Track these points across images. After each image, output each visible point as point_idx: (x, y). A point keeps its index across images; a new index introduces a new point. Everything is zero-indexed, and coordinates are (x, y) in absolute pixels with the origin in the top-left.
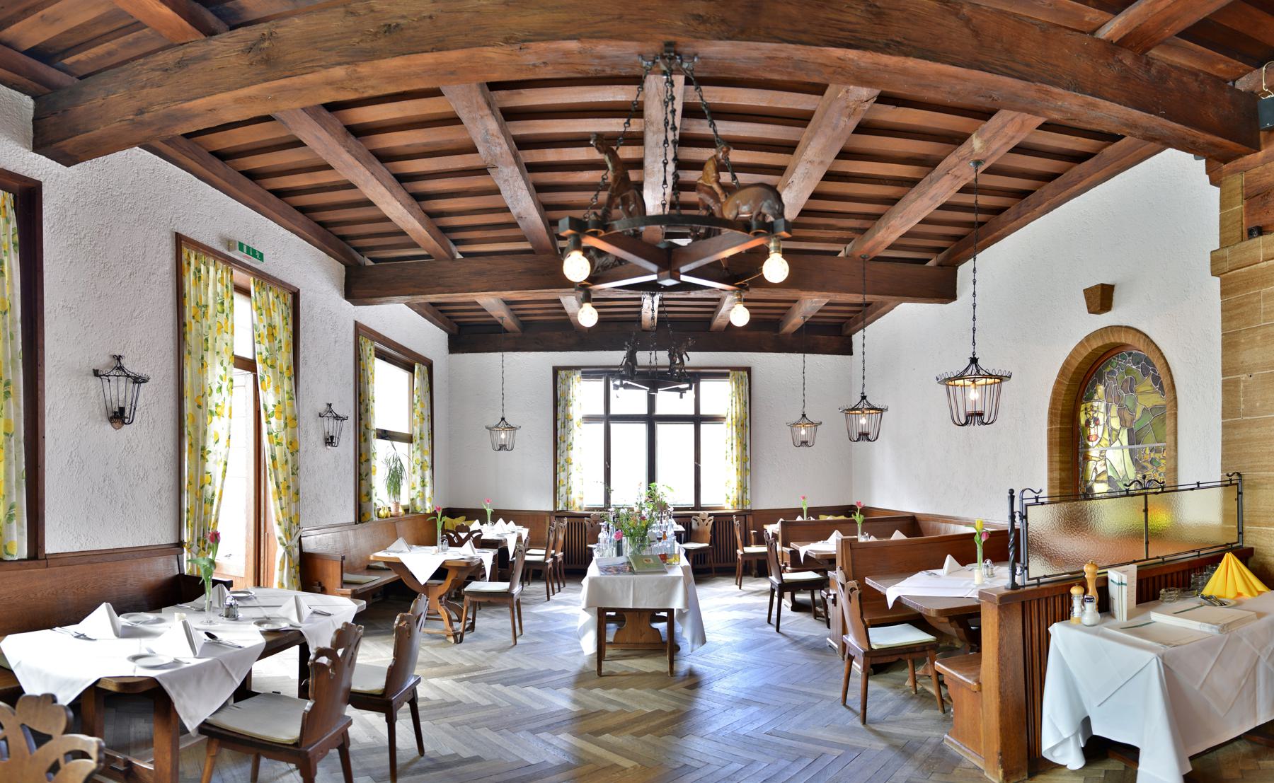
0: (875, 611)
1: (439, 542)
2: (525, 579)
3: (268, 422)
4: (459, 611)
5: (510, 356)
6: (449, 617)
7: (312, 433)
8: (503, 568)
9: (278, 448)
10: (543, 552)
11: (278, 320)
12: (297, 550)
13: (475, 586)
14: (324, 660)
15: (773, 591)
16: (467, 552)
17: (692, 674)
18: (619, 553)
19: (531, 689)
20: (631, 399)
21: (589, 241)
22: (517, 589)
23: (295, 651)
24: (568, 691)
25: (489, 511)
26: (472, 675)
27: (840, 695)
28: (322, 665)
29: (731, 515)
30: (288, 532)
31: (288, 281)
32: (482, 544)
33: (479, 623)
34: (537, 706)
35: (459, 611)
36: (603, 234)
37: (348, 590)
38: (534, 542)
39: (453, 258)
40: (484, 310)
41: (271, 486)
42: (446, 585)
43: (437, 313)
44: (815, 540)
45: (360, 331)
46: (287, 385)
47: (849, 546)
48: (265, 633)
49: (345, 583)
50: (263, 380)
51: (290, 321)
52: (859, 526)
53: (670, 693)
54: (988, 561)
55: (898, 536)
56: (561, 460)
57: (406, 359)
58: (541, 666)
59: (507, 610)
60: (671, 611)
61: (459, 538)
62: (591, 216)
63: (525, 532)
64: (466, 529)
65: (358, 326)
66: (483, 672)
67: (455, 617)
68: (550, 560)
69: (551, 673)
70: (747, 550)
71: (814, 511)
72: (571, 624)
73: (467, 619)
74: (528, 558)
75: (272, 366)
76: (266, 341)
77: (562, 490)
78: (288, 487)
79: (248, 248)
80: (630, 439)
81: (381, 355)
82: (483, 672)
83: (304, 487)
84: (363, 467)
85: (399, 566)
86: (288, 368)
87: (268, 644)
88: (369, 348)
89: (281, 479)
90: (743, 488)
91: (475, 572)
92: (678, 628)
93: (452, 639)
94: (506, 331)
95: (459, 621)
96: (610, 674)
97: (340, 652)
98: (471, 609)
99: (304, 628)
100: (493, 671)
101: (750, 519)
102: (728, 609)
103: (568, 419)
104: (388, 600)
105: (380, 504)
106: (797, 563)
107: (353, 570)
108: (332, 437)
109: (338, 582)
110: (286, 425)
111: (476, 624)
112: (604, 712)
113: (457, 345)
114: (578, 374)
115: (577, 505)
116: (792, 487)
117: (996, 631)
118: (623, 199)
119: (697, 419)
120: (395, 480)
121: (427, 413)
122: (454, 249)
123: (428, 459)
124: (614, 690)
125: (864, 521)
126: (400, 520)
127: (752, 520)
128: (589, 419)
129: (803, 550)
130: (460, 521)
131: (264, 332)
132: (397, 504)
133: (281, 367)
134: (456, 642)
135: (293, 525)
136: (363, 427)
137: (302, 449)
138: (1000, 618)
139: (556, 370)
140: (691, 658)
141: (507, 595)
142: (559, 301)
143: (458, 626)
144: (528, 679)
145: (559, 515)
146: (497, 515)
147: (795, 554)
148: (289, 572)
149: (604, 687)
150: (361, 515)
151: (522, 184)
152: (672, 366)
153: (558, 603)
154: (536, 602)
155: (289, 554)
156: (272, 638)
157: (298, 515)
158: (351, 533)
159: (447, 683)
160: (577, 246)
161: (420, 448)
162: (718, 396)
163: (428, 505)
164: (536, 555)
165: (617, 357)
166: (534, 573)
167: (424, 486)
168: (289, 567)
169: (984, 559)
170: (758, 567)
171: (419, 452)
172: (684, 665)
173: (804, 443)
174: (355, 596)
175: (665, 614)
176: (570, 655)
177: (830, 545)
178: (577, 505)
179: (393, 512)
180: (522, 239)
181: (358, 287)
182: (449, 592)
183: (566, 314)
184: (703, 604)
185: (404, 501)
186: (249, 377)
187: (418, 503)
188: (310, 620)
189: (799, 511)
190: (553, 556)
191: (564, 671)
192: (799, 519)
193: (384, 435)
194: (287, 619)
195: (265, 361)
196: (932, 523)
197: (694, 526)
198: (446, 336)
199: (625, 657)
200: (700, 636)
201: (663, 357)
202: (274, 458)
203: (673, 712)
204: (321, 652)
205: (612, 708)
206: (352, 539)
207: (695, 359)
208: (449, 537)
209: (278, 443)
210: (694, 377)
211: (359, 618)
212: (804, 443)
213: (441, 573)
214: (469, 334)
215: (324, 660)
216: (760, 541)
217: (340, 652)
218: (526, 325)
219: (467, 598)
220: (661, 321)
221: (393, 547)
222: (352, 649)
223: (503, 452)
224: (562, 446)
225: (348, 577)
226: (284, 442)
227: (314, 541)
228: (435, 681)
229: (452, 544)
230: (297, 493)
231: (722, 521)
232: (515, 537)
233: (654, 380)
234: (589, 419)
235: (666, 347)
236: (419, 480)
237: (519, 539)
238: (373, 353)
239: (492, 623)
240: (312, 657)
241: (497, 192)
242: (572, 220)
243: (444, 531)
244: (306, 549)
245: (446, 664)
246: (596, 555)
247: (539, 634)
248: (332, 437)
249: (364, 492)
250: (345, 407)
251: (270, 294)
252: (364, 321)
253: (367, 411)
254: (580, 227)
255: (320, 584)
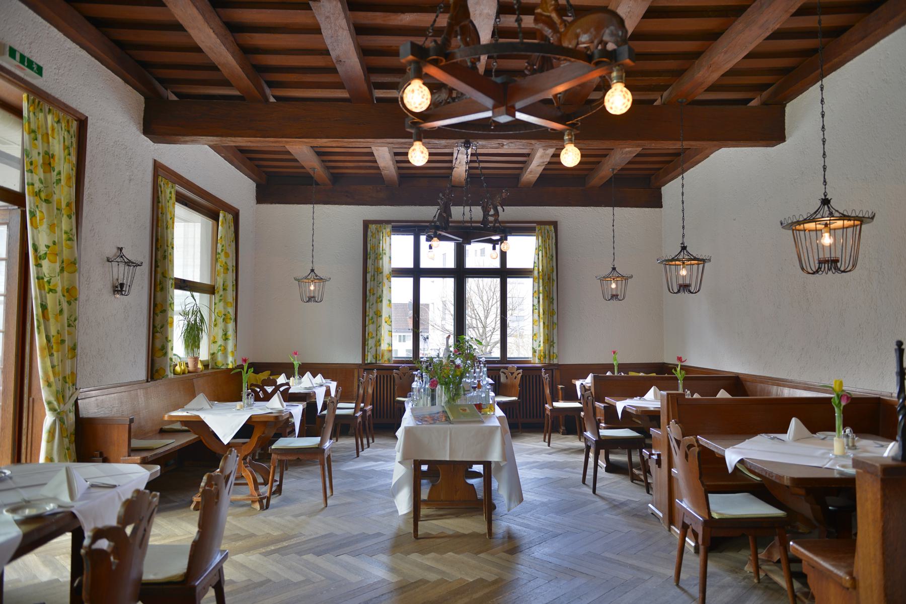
0: (713, 476)
1: (244, 396)
2: (335, 435)
3: (38, 265)
4: (265, 474)
5: (321, 209)
6: (255, 480)
7: (95, 280)
8: (312, 422)
9: (50, 298)
10: (353, 405)
11: (57, 147)
12: (72, 416)
13: (283, 443)
14: (104, 544)
15: (588, 448)
16: (276, 404)
17: (510, 537)
18: (433, 404)
19: (345, 558)
20: (440, 253)
21: (432, 71)
22: (327, 444)
23: (66, 539)
24: (384, 558)
25: (296, 364)
26: (277, 546)
27: (672, 573)
28: (101, 551)
29: (539, 369)
30: (61, 396)
31: (74, 106)
32: (289, 397)
33: (289, 484)
34: (353, 578)
35: (265, 474)
36: (444, 63)
37: (138, 458)
38: (344, 396)
39: (267, 100)
40: (296, 160)
41: (39, 341)
42: (251, 443)
43: (244, 159)
44: (632, 396)
45: (161, 172)
46: (66, 224)
47: (675, 403)
48: (20, 523)
49: (133, 451)
50: (33, 215)
51: (73, 152)
52: (838, 414)
53: (490, 558)
54: (848, 430)
55: (723, 394)
56: (370, 313)
57: (209, 207)
58: (354, 529)
59: (317, 469)
60: (487, 465)
61: (265, 392)
62: (430, 43)
63: (333, 385)
64: (274, 383)
65: (158, 168)
66: (293, 541)
67: (260, 480)
68: (359, 414)
69: (365, 537)
70: (556, 404)
71: (623, 367)
72: (382, 482)
73: (274, 481)
74: (338, 412)
75: (47, 201)
76: (40, 171)
77: (371, 343)
78: (63, 341)
79: (22, 57)
80: (438, 294)
81: (182, 200)
82: (293, 541)
83: (83, 340)
84: (158, 319)
85: (199, 426)
86: (68, 205)
87: (26, 536)
88: (169, 190)
89: (53, 332)
90: (549, 341)
91: (281, 426)
92: (495, 484)
93: (257, 506)
94: (317, 184)
95: (265, 483)
96: (428, 537)
97: (129, 530)
98: (278, 470)
99: (77, 507)
100: (303, 539)
101: (557, 374)
102: (537, 461)
103: (378, 271)
104: (187, 467)
105: (176, 360)
106: (612, 419)
107: (143, 435)
108: (122, 285)
109: (125, 450)
110: (62, 270)
111: (284, 487)
112: (424, 582)
113: (264, 195)
114: (389, 228)
115: (386, 358)
116: (603, 339)
117: (879, 511)
118: (462, 28)
119: (503, 273)
120: (193, 336)
121: (231, 263)
122: (268, 91)
123: (231, 310)
124: (432, 555)
125: (685, 379)
126: (199, 376)
127: (562, 376)
128: (401, 273)
129: (620, 406)
130: (264, 375)
131: (39, 160)
132: (196, 359)
133: (59, 203)
134: (262, 508)
135: (67, 385)
136: (159, 276)
137: (82, 297)
138: (884, 496)
139: (366, 224)
140: (508, 519)
141: (318, 451)
142: (372, 154)
143: (265, 490)
144: (341, 546)
145: (367, 367)
146: (304, 369)
147: (611, 409)
148: (61, 443)
149: (423, 552)
150: (154, 372)
151: (343, 23)
152: (485, 221)
153: (368, 459)
154: (345, 459)
155: (62, 421)
156: (28, 528)
157: (74, 374)
158: (141, 393)
159: (252, 559)
160: (419, 75)
161: (223, 299)
162: (523, 250)
163: (230, 359)
164: (346, 408)
165: (429, 212)
166: (343, 427)
167: (226, 339)
168: (61, 436)
169: (844, 426)
170: (570, 424)
171: (222, 304)
172: (502, 525)
173: (614, 297)
174: (144, 462)
175: (478, 468)
176: (383, 516)
177: (652, 400)
178: (386, 358)
179: (191, 367)
180: (340, 86)
181: (159, 123)
182: (253, 454)
183: (378, 168)
184: (519, 459)
185: (204, 354)
186: (16, 210)
187: (220, 358)
188: (86, 496)
189: (610, 367)
190: (362, 409)
191: (379, 535)
192: (609, 374)
193: (183, 285)
194: (54, 499)
195: (37, 194)
196: (760, 386)
197: (503, 379)
198: (254, 185)
199: (441, 517)
200: (517, 493)
201: (477, 212)
202: (44, 307)
203: (495, 582)
204: (99, 534)
205: (433, 577)
206: (142, 400)
207: (509, 213)
208: (253, 391)
209: (51, 290)
210: (506, 230)
211: (152, 485)
212: (614, 297)
213: (246, 431)
214: (278, 184)
215: (104, 544)
216: (570, 395)
217: (129, 530)
218: (336, 178)
219: (274, 456)
220: (472, 175)
221: (193, 404)
222: (144, 523)
223: (312, 304)
224: (371, 299)
225: (136, 443)
226: (59, 289)
227: (95, 403)
228: (239, 558)
229: (257, 399)
230: (74, 348)
231: (530, 374)
232: (324, 389)
233: (465, 234)
234: (401, 273)
235: (467, 205)
236: (220, 333)
237: (328, 392)
238: (174, 196)
239: (301, 484)
240: (86, 542)
241: (317, 30)
242: (413, 45)
243: (251, 386)
244: (84, 414)
245: (252, 535)
246: (408, 407)
247: (350, 494)
248: (122, 285)
249: (158, 345)
250: (139, 251)
251: (50, 118)
252: (163, 161)
253: (165, 257)
254: (420, 53)
255: (101, 454)
